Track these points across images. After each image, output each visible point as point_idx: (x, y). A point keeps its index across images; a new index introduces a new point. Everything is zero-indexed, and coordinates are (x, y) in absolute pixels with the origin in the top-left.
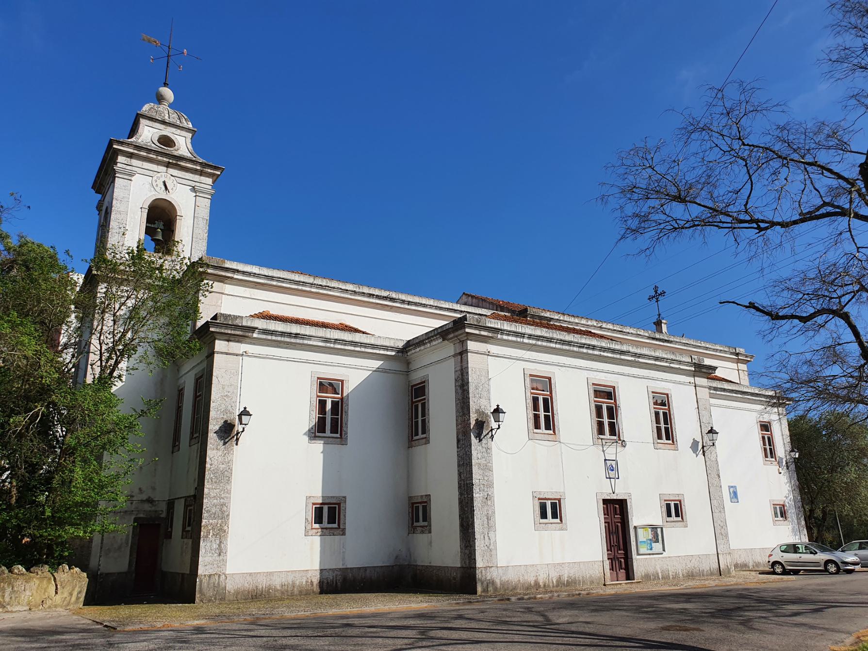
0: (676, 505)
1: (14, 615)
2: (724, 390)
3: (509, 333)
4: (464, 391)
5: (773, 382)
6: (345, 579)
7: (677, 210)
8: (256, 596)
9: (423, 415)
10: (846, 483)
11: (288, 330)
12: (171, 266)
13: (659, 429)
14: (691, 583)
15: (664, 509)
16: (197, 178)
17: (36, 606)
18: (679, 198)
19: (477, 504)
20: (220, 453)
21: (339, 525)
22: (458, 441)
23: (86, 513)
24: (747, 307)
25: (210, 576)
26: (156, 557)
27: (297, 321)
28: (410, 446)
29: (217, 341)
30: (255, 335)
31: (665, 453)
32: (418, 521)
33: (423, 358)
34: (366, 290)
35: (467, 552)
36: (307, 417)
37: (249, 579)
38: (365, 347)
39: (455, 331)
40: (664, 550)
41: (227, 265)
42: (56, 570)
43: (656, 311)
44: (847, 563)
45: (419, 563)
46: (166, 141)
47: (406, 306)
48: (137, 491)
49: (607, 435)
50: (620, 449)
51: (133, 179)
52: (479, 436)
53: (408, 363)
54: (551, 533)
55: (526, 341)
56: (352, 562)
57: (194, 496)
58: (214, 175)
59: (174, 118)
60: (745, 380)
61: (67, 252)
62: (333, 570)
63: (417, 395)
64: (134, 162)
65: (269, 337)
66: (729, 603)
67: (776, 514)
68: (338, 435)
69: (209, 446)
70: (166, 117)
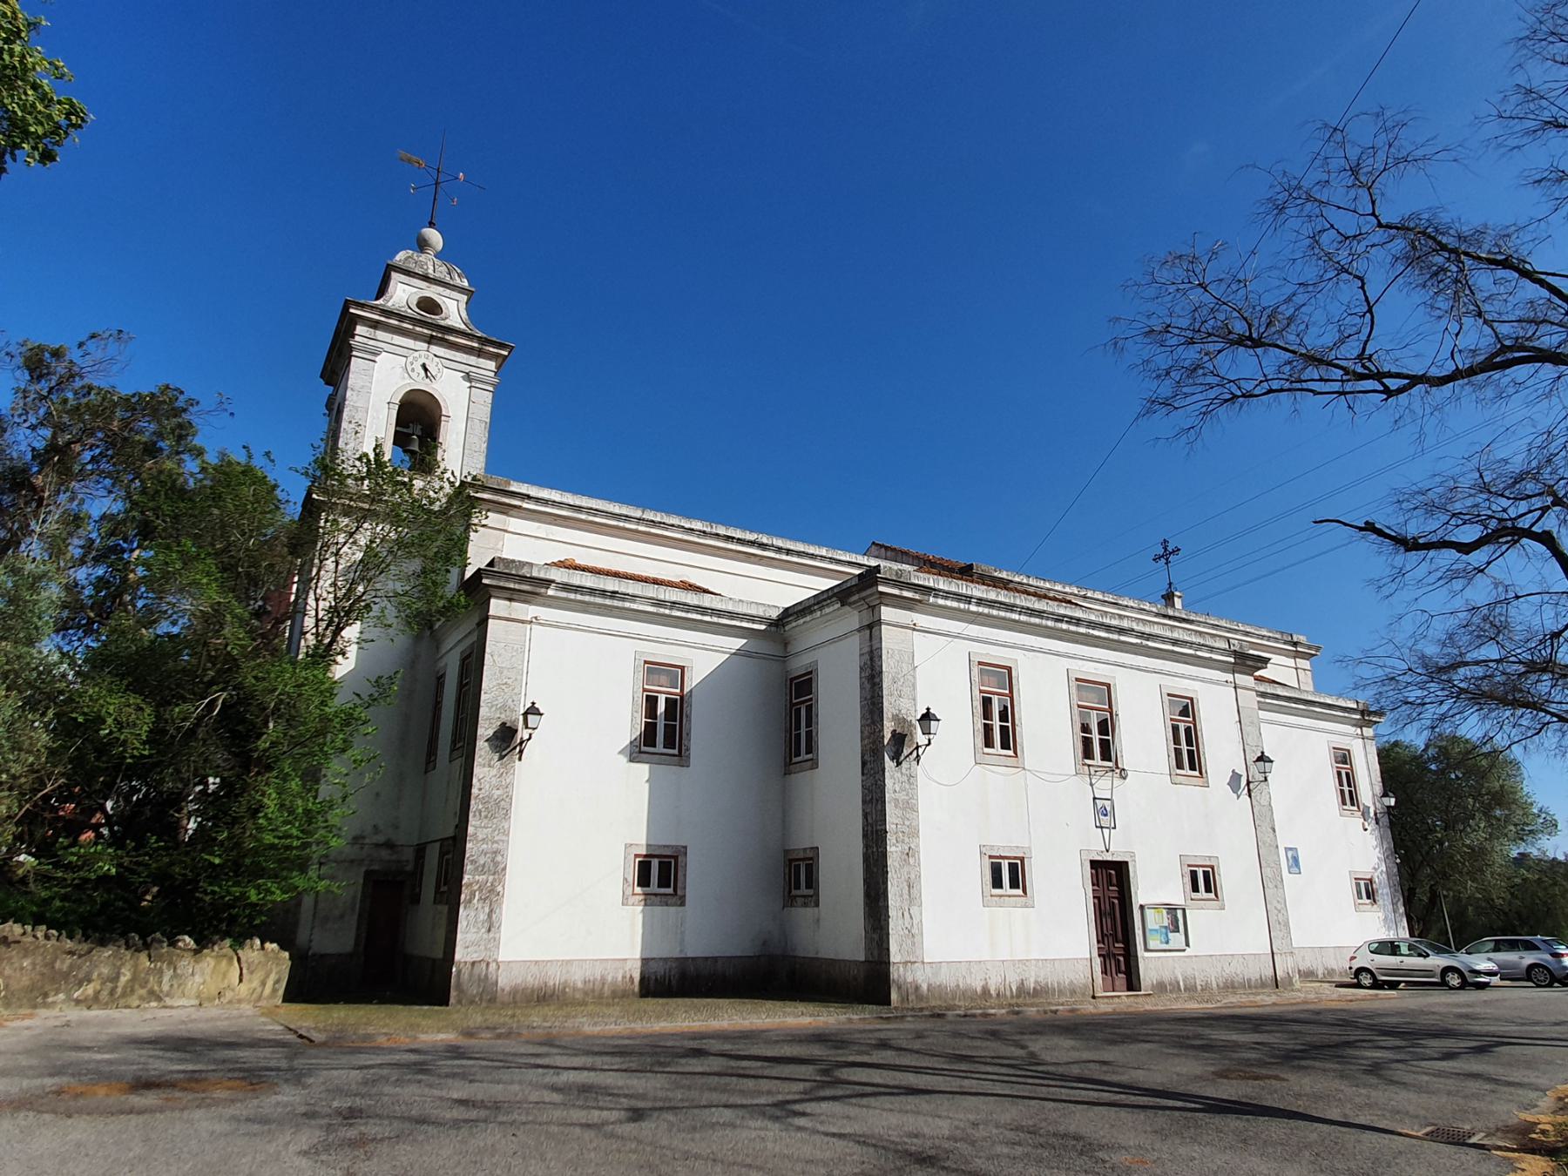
0: (1206, 874)
1: (174, 1012)
2: (1277, 697)
3: (948, 595)
4: (874, 685)
5: (1380, 672)
6: (683, 976)
7: (1243, 365)
8: (543, 997)
9: (809, 724)
10: (1468, 847)
11: (601, 586)
12: (434, 491)
14: (1233, 999)
15: (1188, 879)
16: (473, 360)
19: (893, 862)
20: (494, 772)
22: (864, 764)
24: (1361, 529)
25: (473, 963)
26: (388, 932)
28: (787, 773)
29: (493, 601)
30: (550, 592)
31: (1188, 791)
32: (798, 887)
34: (722, 531)
35: (876, 936)
36: (627, 723)
37: (534, 969)
38: (719, 616)
39: (860, 592)
41: (512, 489)
42: (241, 945)
43: (1165, 574)
46: (429, 305)
47: (784, 557)
49: (1097, 760)
50: (1117, 781)
51: (377, 359)
52: (896, 757)
54: (1009, 913)
56: (696, 947)
57: (454, 838)
58: (498, 355)
59: (441, 272)
60: (1307, 683)
61: (267, 454)
62: (665, 960)
63: (801, 688)
64: (380, 335)
65: (572, 596)
67: (1359, 893)
68: (676, 752)
69: (478, 760)
70: (431, 271)
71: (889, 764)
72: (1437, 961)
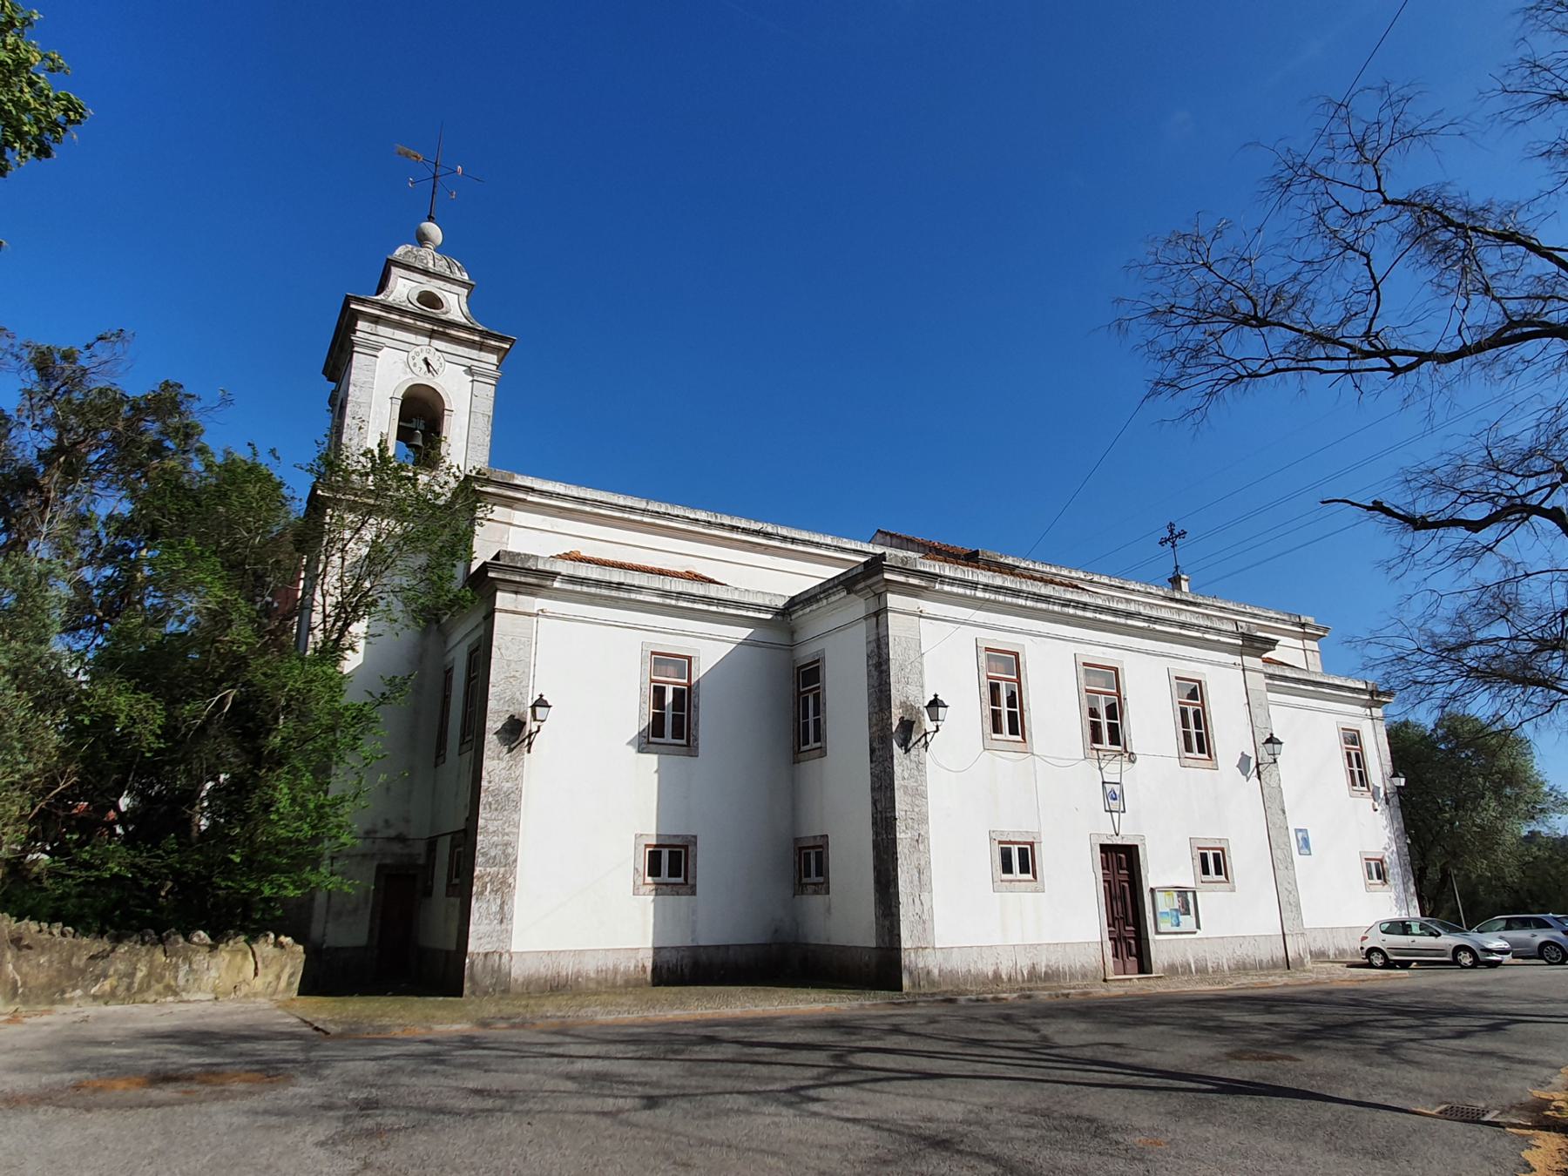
0: (1216, 856)
2: (1285, 678)
3: (954, 581)
4: (881, 672)
6: (696, 964)
7: (1249, 345)
8: (557, 987)
9: (817, 712)
10: (1478, 826)
11: (607, 578)
12: (439, 484)
13: (1187, 736)
14: (1245, 980)
15: (1198, 862)
16: (474, 353)
17: (227, 994)
18: (1259, 321)
19: (902, 849)
20: (503, 764)
21: (686, 879)
22: (872, 751)
23: (302, 856)
24: (1369, 509)
25: (486, 955)
26: (403, 924)
27: (621, 566)
28: (796, 761)
29: (499, 594)
30: (556, 585)
31: (1197, 774)
32: (808, 875)
33: (815, 623)
34: (727, 520)
36: (634, 715)
37: (546, 959)
39: (865, 580)
40: (1198, 927)
43: (1172, 556)
44: (1490, 951)
47: (789, 546)
48: (380, 824)
49: (1106, 744)
50: (1126, 766)
52: (905, 745)
53: (792, 632)
55: (980, 594)
57: (465, 831)
59: (441, 266)
60: (1316, 664)
61: (273, 451)
63: (808, 677)
64: (381, 330)
65: (578, 588)
66: (1346, 1015)
67: (1370, 873)
68: (684, 742)
69: (487, 753)
71: (897, 751)
72: (1448, 941)
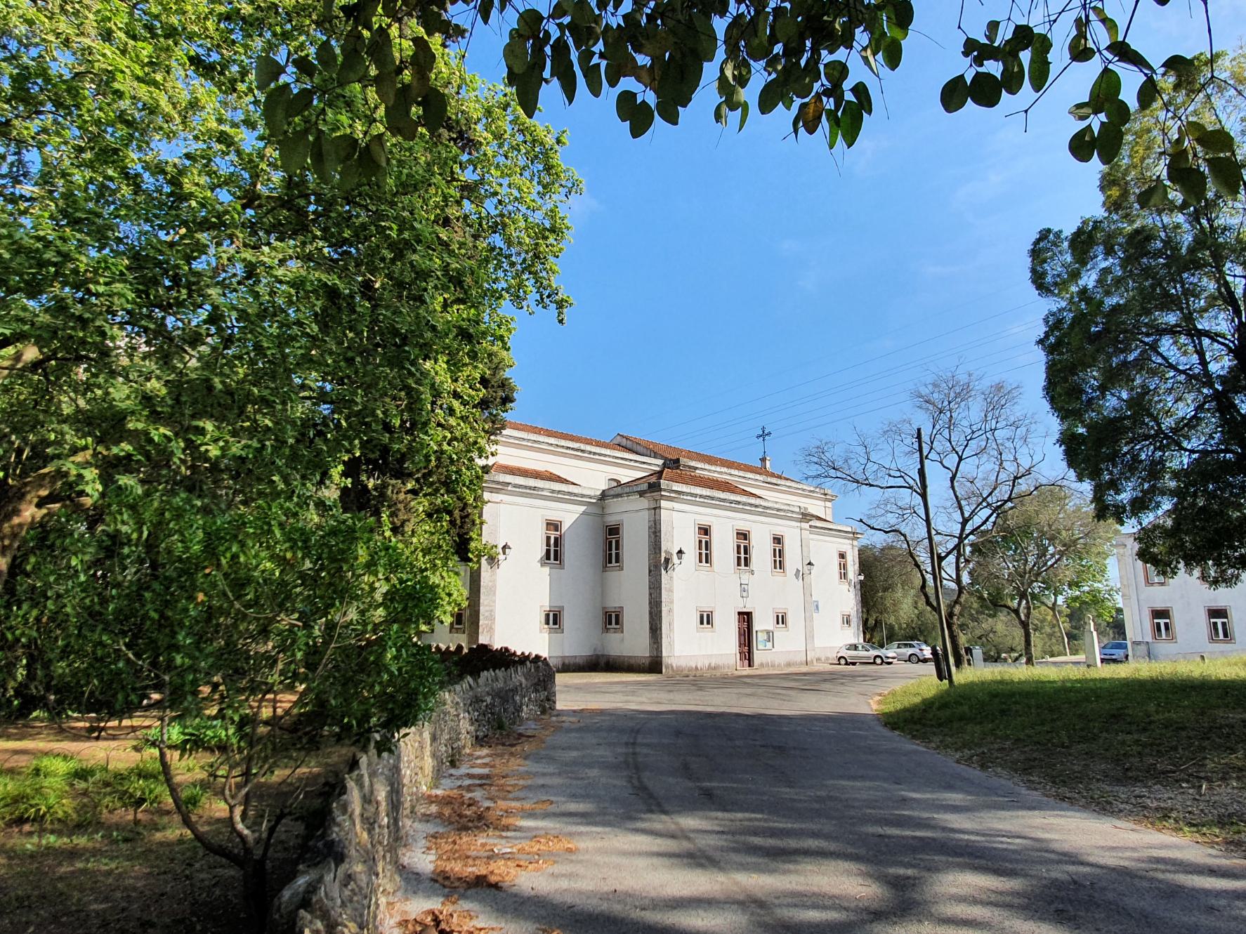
9: (617, 548)
31: (778, 577)
32: (610, 623)
45: (612, 653)
52: (666, 569)
63: (614, 531)
71: (663, 572)
72: (874, 653)
